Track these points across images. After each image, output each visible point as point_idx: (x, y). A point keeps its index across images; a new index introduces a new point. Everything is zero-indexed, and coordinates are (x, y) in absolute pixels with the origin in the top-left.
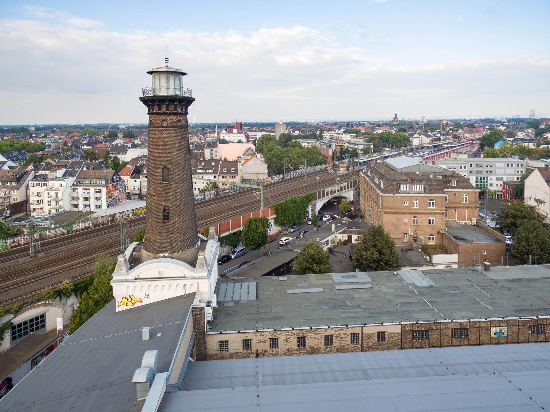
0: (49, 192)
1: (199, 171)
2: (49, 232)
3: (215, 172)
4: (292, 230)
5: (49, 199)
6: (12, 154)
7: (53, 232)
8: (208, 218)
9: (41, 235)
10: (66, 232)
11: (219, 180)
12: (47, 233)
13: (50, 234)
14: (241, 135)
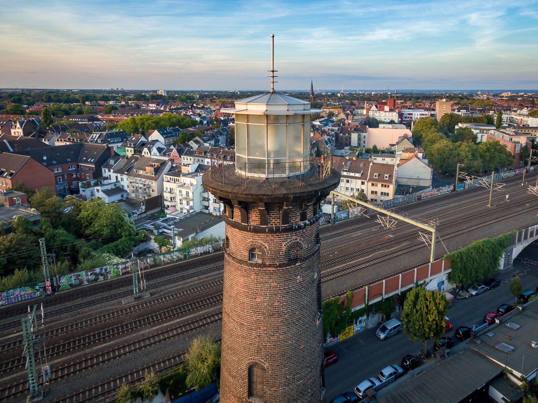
0: (181, 189)
2: (164, 257)
5: (180, 197)
6: (167, 131)
8: (352, 258)
9: (155, 260)
11: (368, 188)
13: (165, 259)
14: (395, 113)
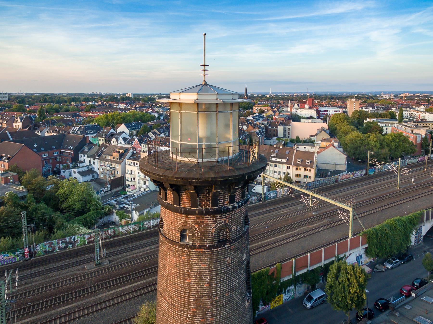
1: (273, 159)
2: (122, 229)
3: (289, 162)
4: (389, 266)
6: (131, 124)
7: (126, 228)
8: (280, 233)
9: (115, 231)
10: (137, 229)
11: (293, 171)
12: (120, 229)
13: (123, 230)
